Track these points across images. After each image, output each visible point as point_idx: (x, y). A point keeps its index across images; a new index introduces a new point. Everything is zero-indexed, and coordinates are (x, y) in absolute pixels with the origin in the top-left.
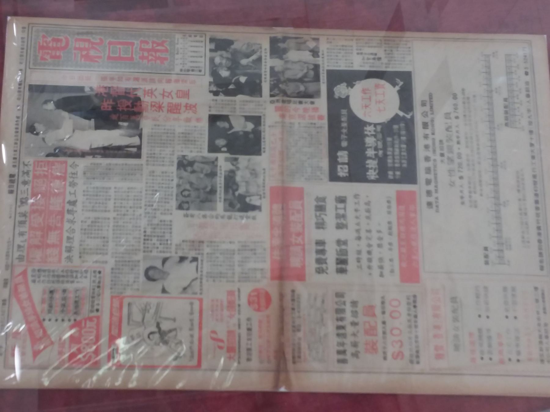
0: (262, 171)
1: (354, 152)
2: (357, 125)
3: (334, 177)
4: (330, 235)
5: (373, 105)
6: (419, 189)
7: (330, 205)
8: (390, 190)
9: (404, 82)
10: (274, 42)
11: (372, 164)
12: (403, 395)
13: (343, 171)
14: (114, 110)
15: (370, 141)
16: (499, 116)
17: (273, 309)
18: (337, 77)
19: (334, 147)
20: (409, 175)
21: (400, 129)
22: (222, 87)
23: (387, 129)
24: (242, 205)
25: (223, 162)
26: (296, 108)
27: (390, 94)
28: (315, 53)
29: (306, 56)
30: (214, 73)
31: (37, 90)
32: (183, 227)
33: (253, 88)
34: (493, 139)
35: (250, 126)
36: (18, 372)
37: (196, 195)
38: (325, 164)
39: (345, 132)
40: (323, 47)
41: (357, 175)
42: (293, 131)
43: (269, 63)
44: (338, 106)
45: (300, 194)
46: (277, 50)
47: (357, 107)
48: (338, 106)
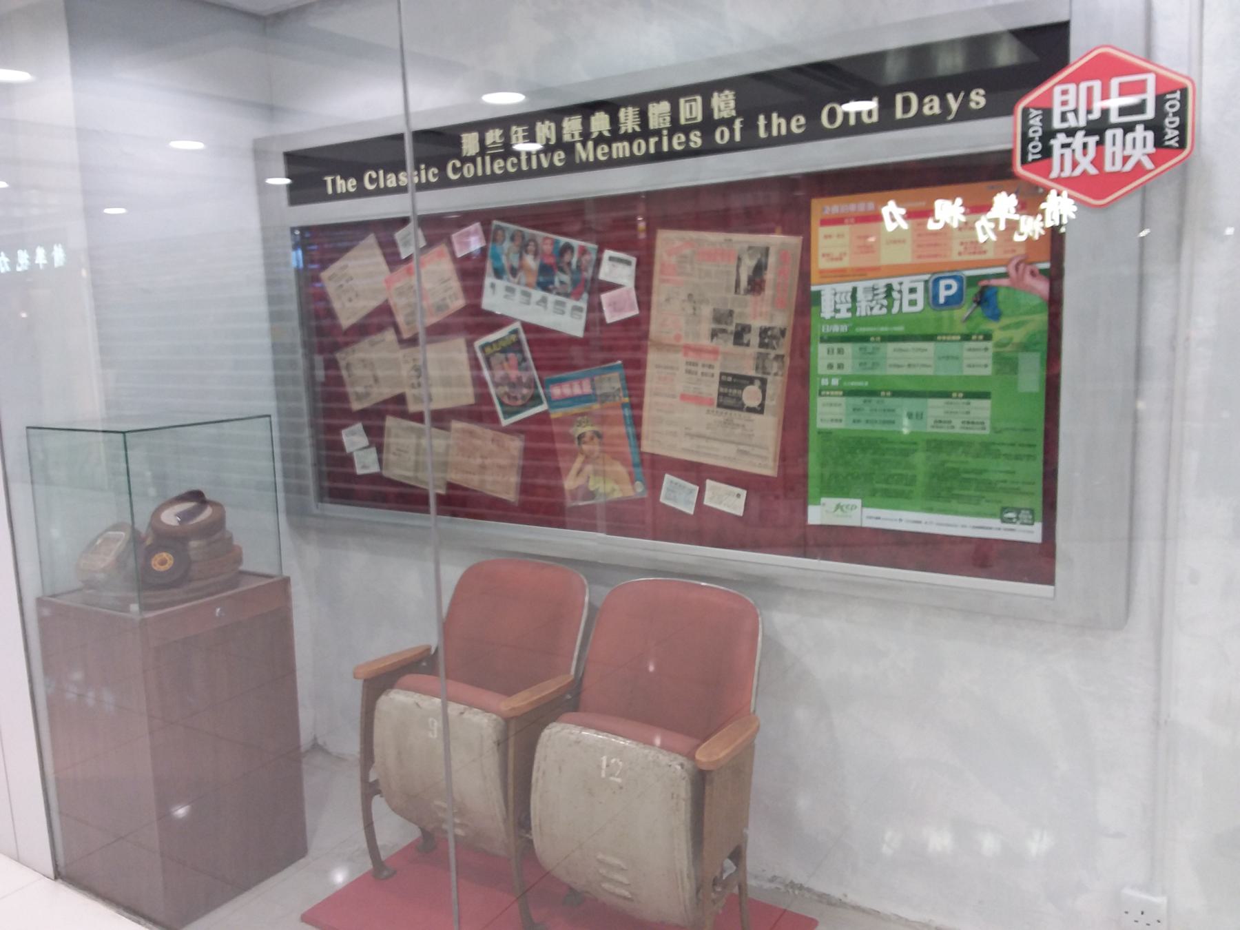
0: (726, 345)
1: (732, 384)
2: (742, 387)
3: (722, 374)
4: (700, 370)
5: (751, 396)
6: (715, 408)
7: (711, 371)
8: (715, 396)
9: (760, 410)
10: (783, 356)
11: (726, 390)
12: (588, 199)
13: (724, 378)
14: (756, 284)
15: (735, 391)
16: (742, 447)
17: (673, 342)
18: (764, 382)
19: (734, 376)
20: (720, 405)
21: (739, 406)
22: (764, 332)
23: (739, 399)
24: (714, 334)
25: (732, 328)
26: (752, 363)
27: (754, 403)
28: (776, 374)
29: (775, 370)
30: (769, 328)
31: (766, 251)
32: (707, 311)
33: (762, 345)
34: (732, 442)
35: (745, 341)
36: (123, 534)
37: (721, 317)
38: (728, 371)
39: (740, 381)
40: (779, 378)
41: (722, 383)
42: (744, 361)
43: (773, 353)
44: (751, 380)
45: (716, 359)
46: (778, 357)
47: (749, 388)
48: (751, 380)
